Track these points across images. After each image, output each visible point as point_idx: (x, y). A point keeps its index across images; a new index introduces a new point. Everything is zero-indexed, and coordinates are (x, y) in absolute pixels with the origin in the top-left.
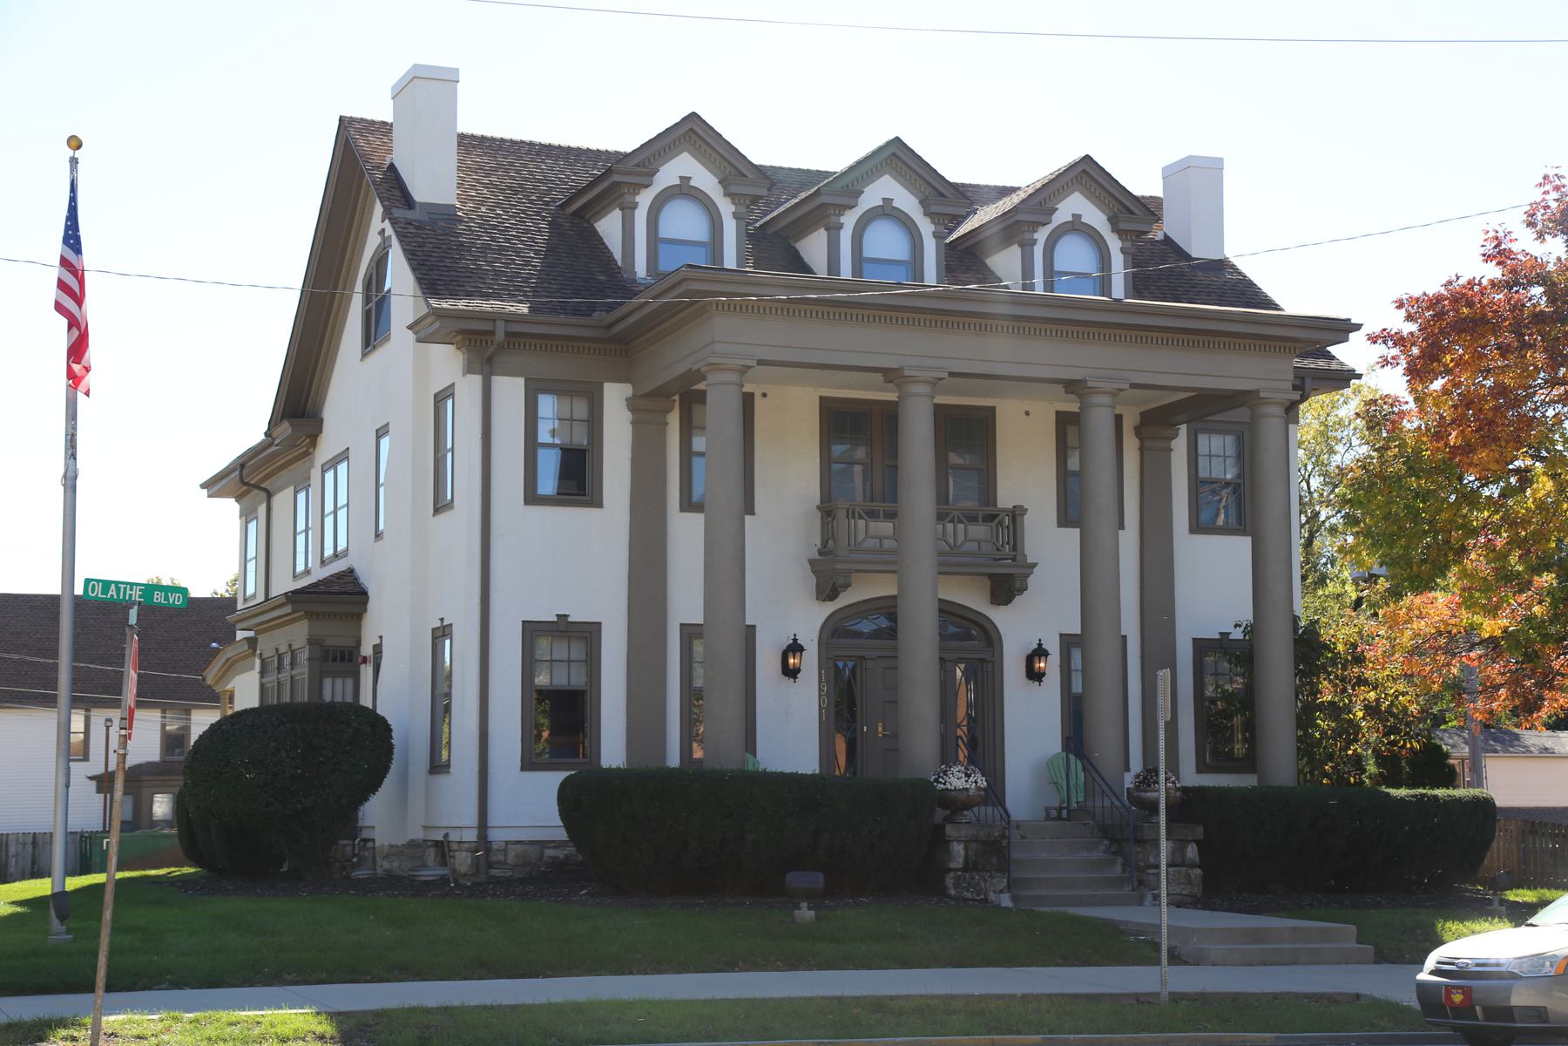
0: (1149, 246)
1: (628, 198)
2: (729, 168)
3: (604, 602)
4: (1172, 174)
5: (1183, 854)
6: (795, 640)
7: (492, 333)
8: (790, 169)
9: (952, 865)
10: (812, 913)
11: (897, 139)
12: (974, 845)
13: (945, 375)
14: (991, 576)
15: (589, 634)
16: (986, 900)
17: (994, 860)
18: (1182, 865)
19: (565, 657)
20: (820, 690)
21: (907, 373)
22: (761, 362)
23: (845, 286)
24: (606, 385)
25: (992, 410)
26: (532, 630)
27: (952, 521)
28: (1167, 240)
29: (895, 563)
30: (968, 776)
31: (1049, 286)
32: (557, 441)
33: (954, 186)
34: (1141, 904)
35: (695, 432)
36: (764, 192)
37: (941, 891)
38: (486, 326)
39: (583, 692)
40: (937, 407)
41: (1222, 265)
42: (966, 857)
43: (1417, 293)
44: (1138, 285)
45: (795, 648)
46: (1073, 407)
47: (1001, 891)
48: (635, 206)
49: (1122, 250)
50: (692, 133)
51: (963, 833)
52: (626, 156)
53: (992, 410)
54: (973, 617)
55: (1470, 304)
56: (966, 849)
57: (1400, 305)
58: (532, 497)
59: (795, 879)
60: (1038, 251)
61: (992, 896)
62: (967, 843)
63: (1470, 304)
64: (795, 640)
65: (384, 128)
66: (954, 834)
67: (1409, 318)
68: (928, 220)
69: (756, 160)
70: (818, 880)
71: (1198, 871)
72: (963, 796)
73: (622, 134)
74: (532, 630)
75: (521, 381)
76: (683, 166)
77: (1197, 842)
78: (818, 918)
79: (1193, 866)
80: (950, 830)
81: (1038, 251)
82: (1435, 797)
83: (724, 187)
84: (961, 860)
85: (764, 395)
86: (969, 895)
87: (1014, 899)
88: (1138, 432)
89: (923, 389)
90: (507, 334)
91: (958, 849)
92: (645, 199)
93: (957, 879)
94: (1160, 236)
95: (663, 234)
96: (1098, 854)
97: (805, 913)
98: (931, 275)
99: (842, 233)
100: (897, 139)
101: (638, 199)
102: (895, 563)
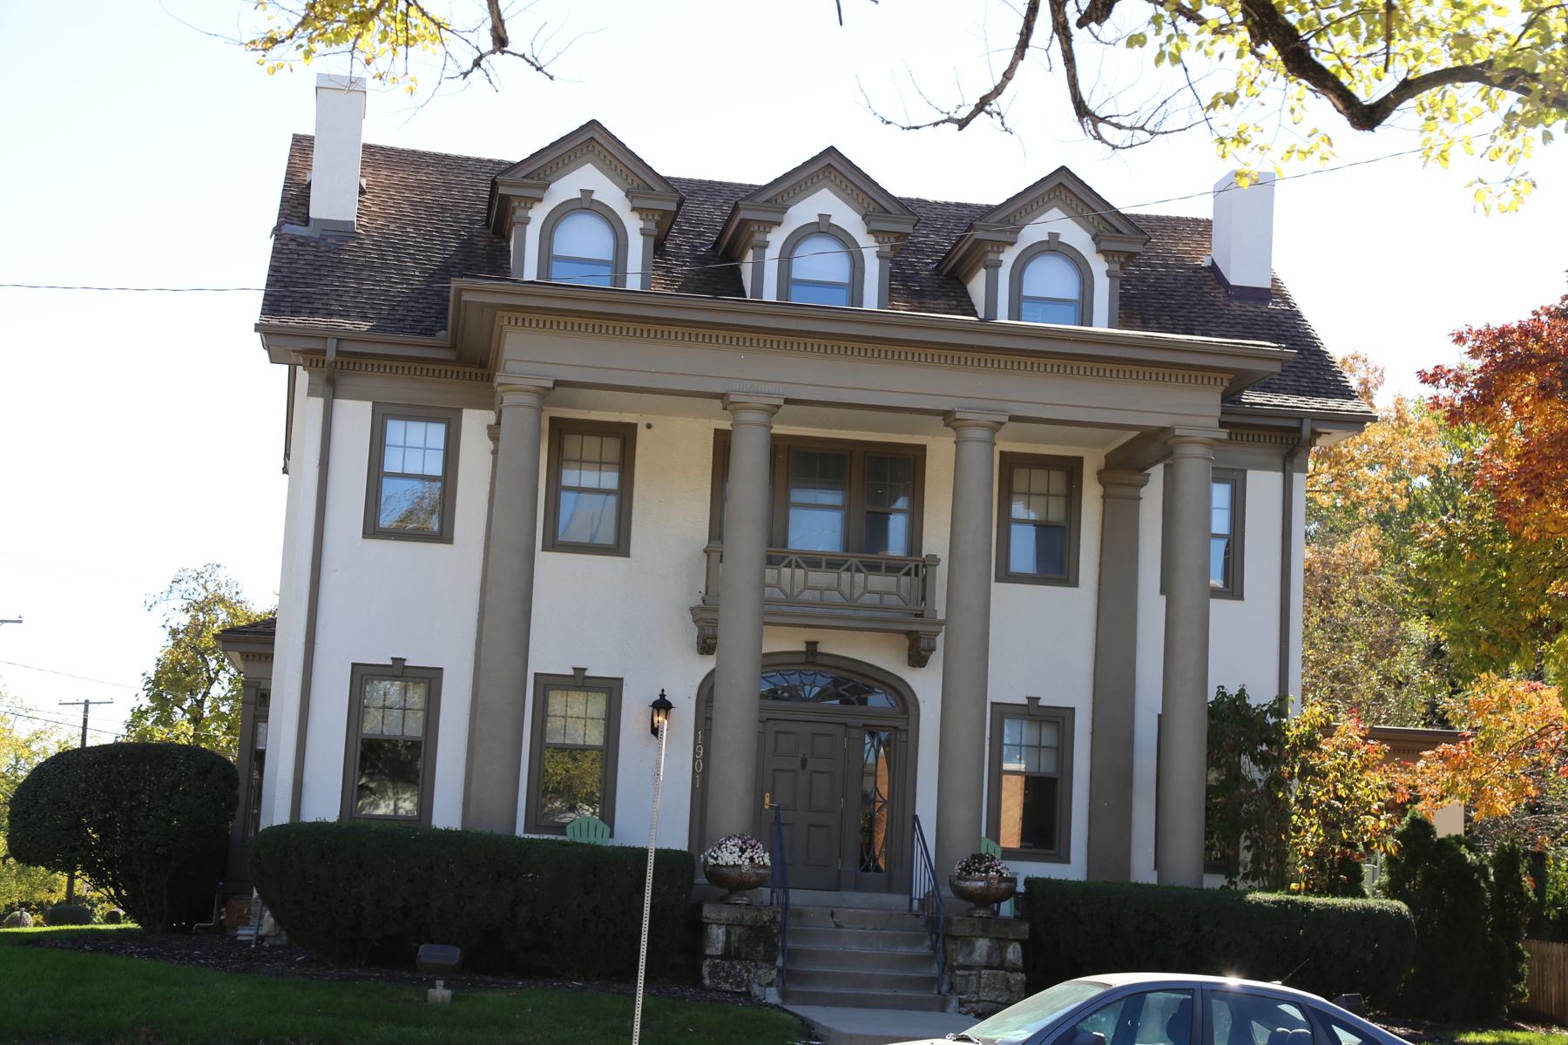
0: (1190, 273)
1: (991, 256)
2: (636, 182)
3: (1071, 688)
4: (1223, 190)
5: (1002, 955)
6: (662, 696)
7: (323, 352)
8: (700, 182)
9: (708, 952)
10: (447, 993)
11: (594, 123)
12: (738, 930)
13: (781, 402)
14: (909, 634)
15: (431, 679)
16: (748, 993)
17: (761, 948)
18: (1001, 967)
19: (582, 714)
20: (695, 753)
21: (1178, 432)
22: (1013, 419)
23: (870, 318)
24: (1250, 474)
25: (922, 449)
26: (363, 675)
27: (848, 569)
28: (1214, 268)
29: (767, 613)
30: (743, 851)
31: (1015, 312)
32: (1033, 516)
33: (1126, 218)
34: (943, 1009)
35: (1015, 497)
36: (909, 229)
37: (697, 980)
38: (1294, 424)
39: (1054, 780)
40: (774, 437)
41: (1273, 293)
42: (728, 943)
43: (1479, 325)
44: (1129, 308)
45: (662, 705)
46: (725, 425)
47: (770, 985)
48: (999, 264)
49: (1109, 274)
50: (591, 142)
51: (724, 915)
52: (513, 166)
53: (922, 449)
54: (890, 681)
55: (1538, 338)
56: (728, 934)
57: (1460, 339)
58: (372, 529)
59: (428, 954)
60: (1004, 275)
61: (756, 990)
62: (729, 926)
63: (1538, 338)
64: (662, 696)
65: (1201, 228)
66: (713, 915)
67: (1475, 353)
68: (1101, 258)
69: (897, 192)
70: (453, 955)
71: (1021, 977)
72: (734, 873)
73: (757, 167)
74: (363, 675)
75: (369, 405)
76: (824, 203)
77: (1022, 942)
78: (453, 998)
79: (1014, 969)
80: (708, 911)
81: (1004, 275)
82: (1309, 905)
83: (1097, 244)
84: (720, 946)
85: (649, 426)
86: (727, 987)
87: (784, 995)
88: (1101, 476)
89: (982, 434)
90: (339, 353)
91: (718, 934)
92: (1009, 257)
93: (714, 967)
94: (1205, 262)
95: (797, 273)
96: (923, 949)
97: (440, 992)
98: (871, 301)
99: (1001, 270)
100: (832, 151)
101: (769, 237)
102: (767, 613)
